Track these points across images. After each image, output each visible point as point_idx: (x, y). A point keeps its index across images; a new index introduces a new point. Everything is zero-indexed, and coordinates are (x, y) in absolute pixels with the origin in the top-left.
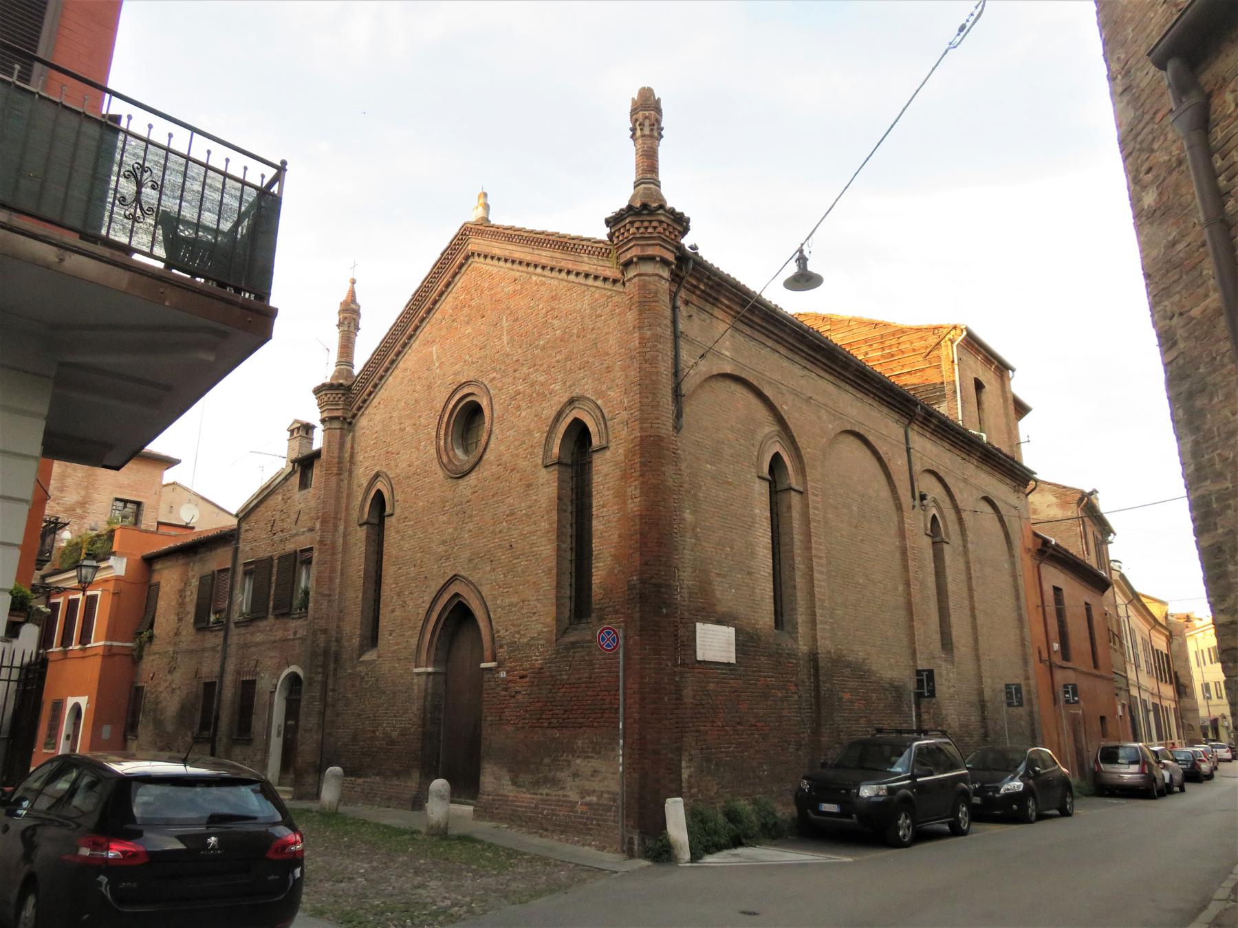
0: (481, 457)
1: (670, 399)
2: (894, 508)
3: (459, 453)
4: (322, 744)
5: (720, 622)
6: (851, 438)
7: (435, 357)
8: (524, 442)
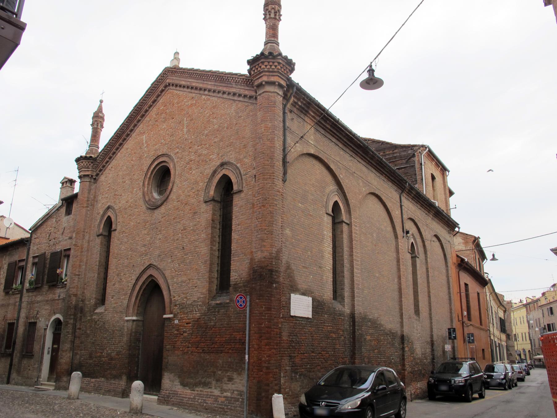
0: (168, 196)
1: (281, 163)
2: (393, 237)
3: (156, 195)
4: (72, 359)
5: (303, 294)
6: (374, 197)
7: (144, 141)
8: (193, 189)
